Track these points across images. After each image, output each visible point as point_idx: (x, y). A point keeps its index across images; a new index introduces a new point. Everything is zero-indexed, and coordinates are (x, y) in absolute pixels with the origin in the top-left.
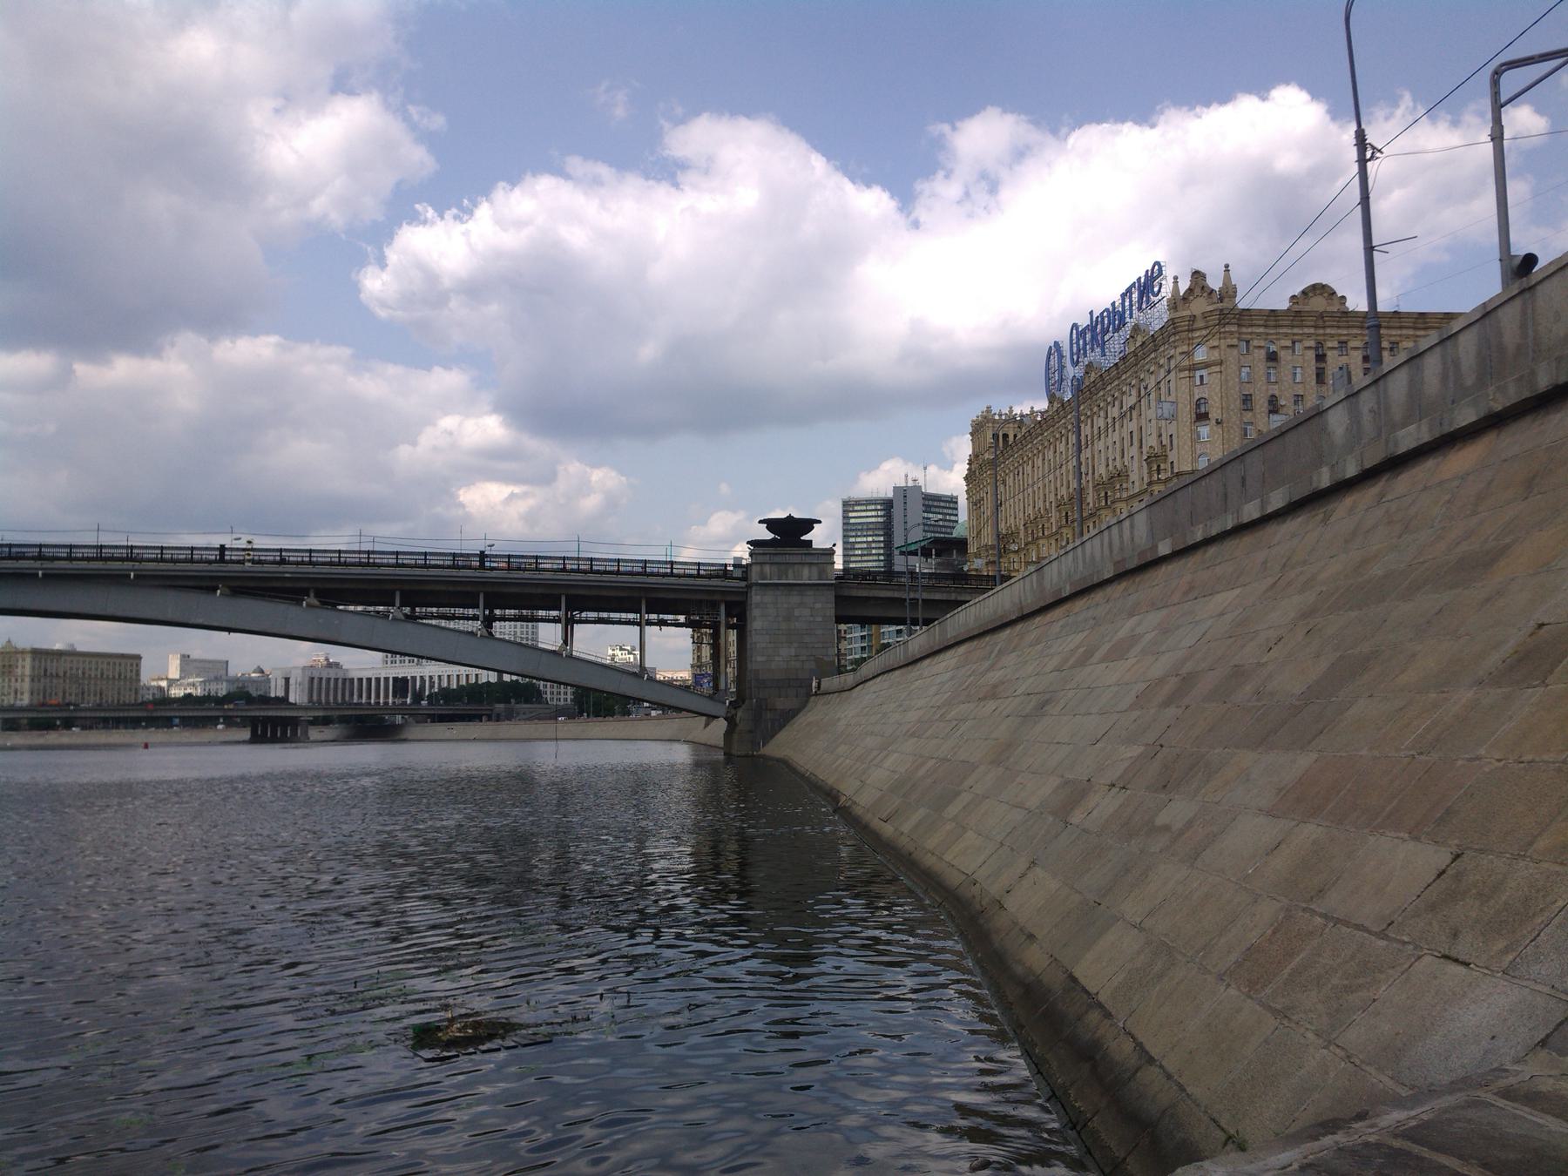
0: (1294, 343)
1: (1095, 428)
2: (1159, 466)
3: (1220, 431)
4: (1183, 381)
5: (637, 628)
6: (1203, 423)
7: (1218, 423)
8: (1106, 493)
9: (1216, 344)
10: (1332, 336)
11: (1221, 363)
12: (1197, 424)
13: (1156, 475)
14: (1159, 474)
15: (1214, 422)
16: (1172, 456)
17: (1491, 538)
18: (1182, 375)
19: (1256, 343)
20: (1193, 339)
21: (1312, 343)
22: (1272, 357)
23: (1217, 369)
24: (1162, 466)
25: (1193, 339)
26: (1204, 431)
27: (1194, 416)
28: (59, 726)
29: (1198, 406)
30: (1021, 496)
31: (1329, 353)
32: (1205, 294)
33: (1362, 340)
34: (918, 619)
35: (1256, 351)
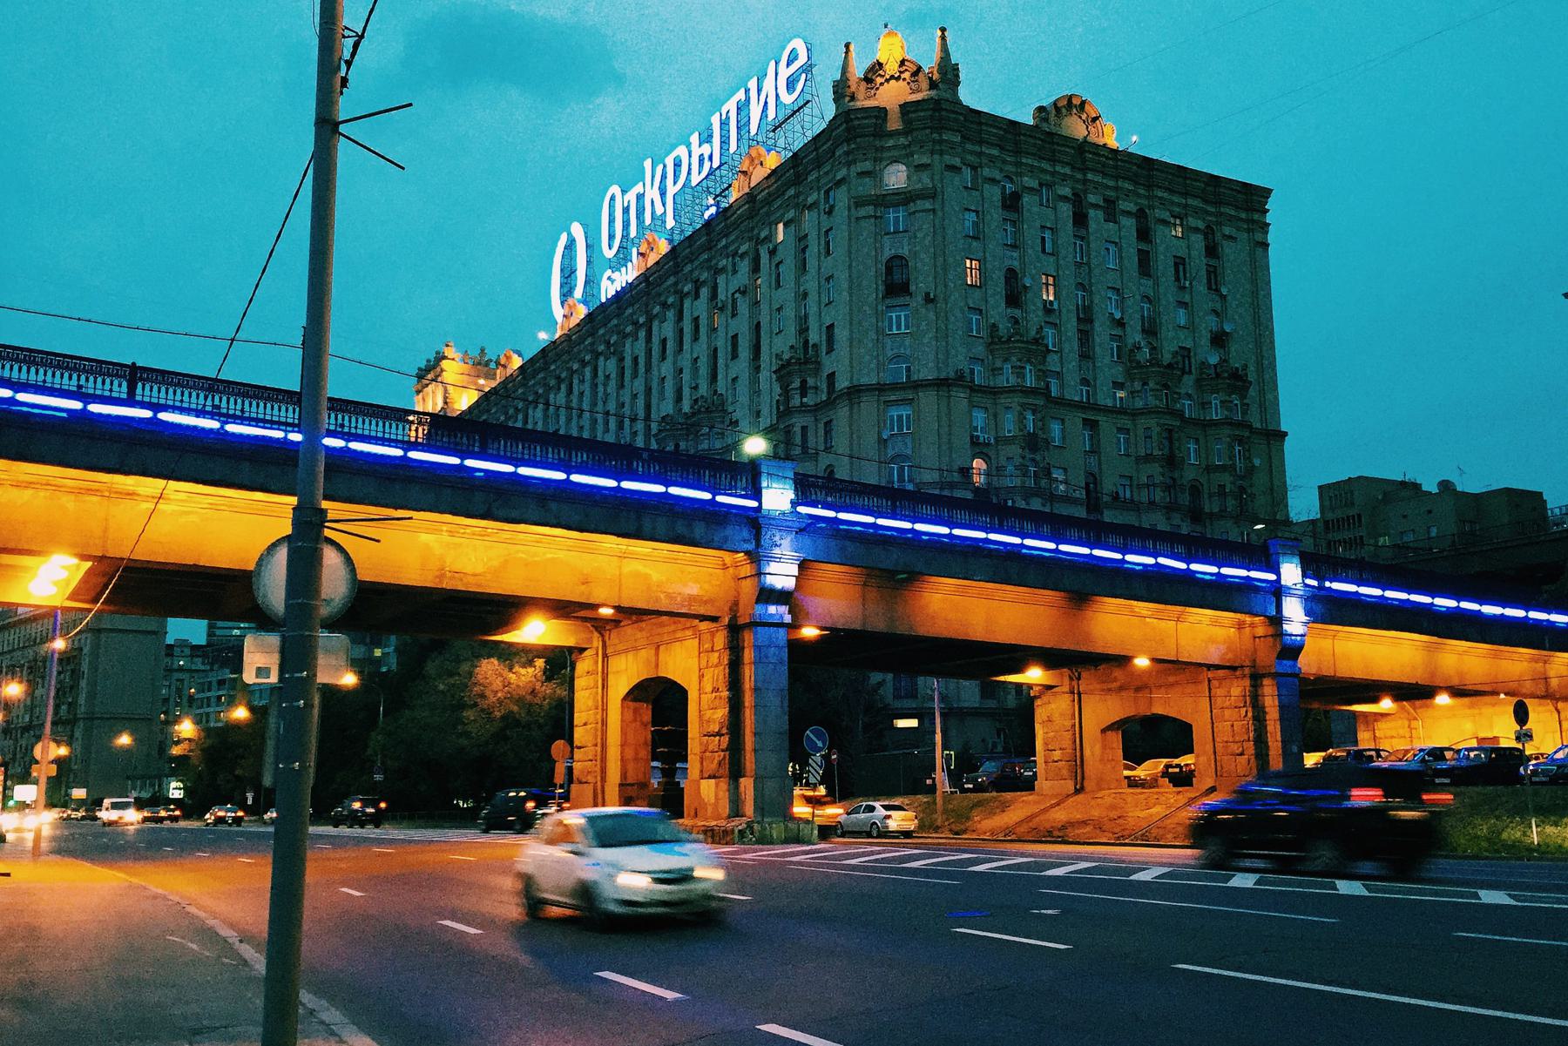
0: (1041, 185)
1: (656, 341)
2: (804, 382)
3: (932, 316)
4: (863, 223)
5: (339, 383)
6: (901, 301)
7: (928, 300)
8: (804, 382)
9: (925, 160)
10: (1097, 185)
11: (933, 196)
12: (888, 302)
13: (797, 397)
14: (803, 395)
15: (920, 299)
16: (828, 365)
17: (1115, 685)
18: (863, 212)
19: (986, 172)
20: (883, 149)
21: (1066, 191)
22: (1012, 203)
23: (928, 205)
24: (811, 382)
25: (883, 149)
26: (899, 320)
27: (882, 288)
28: (11, 808)
29: (889, 270)
30: (666, 369)
31: (1092, 213)
32: (907, 75)
33: (1136, 204)
35: (986, 186)
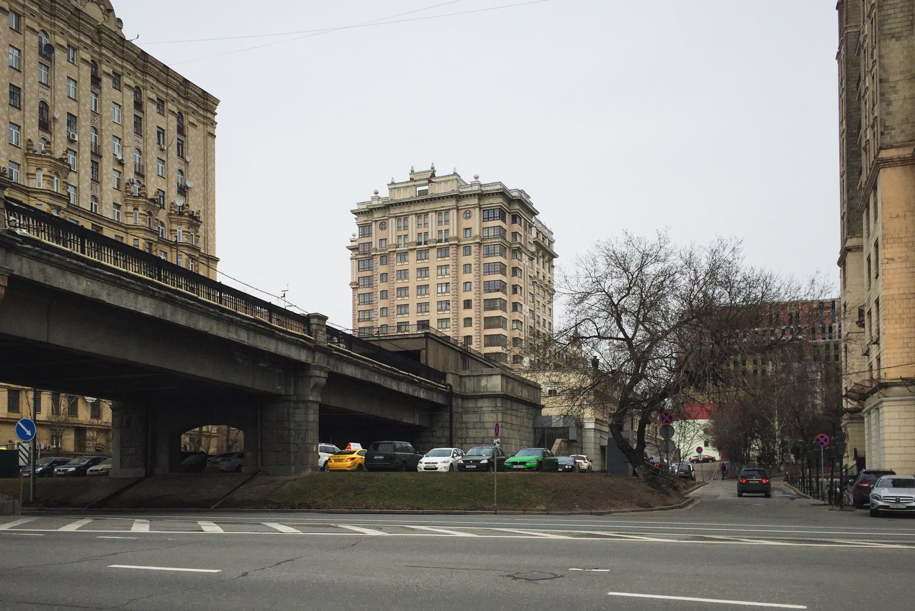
34: (442, 240)
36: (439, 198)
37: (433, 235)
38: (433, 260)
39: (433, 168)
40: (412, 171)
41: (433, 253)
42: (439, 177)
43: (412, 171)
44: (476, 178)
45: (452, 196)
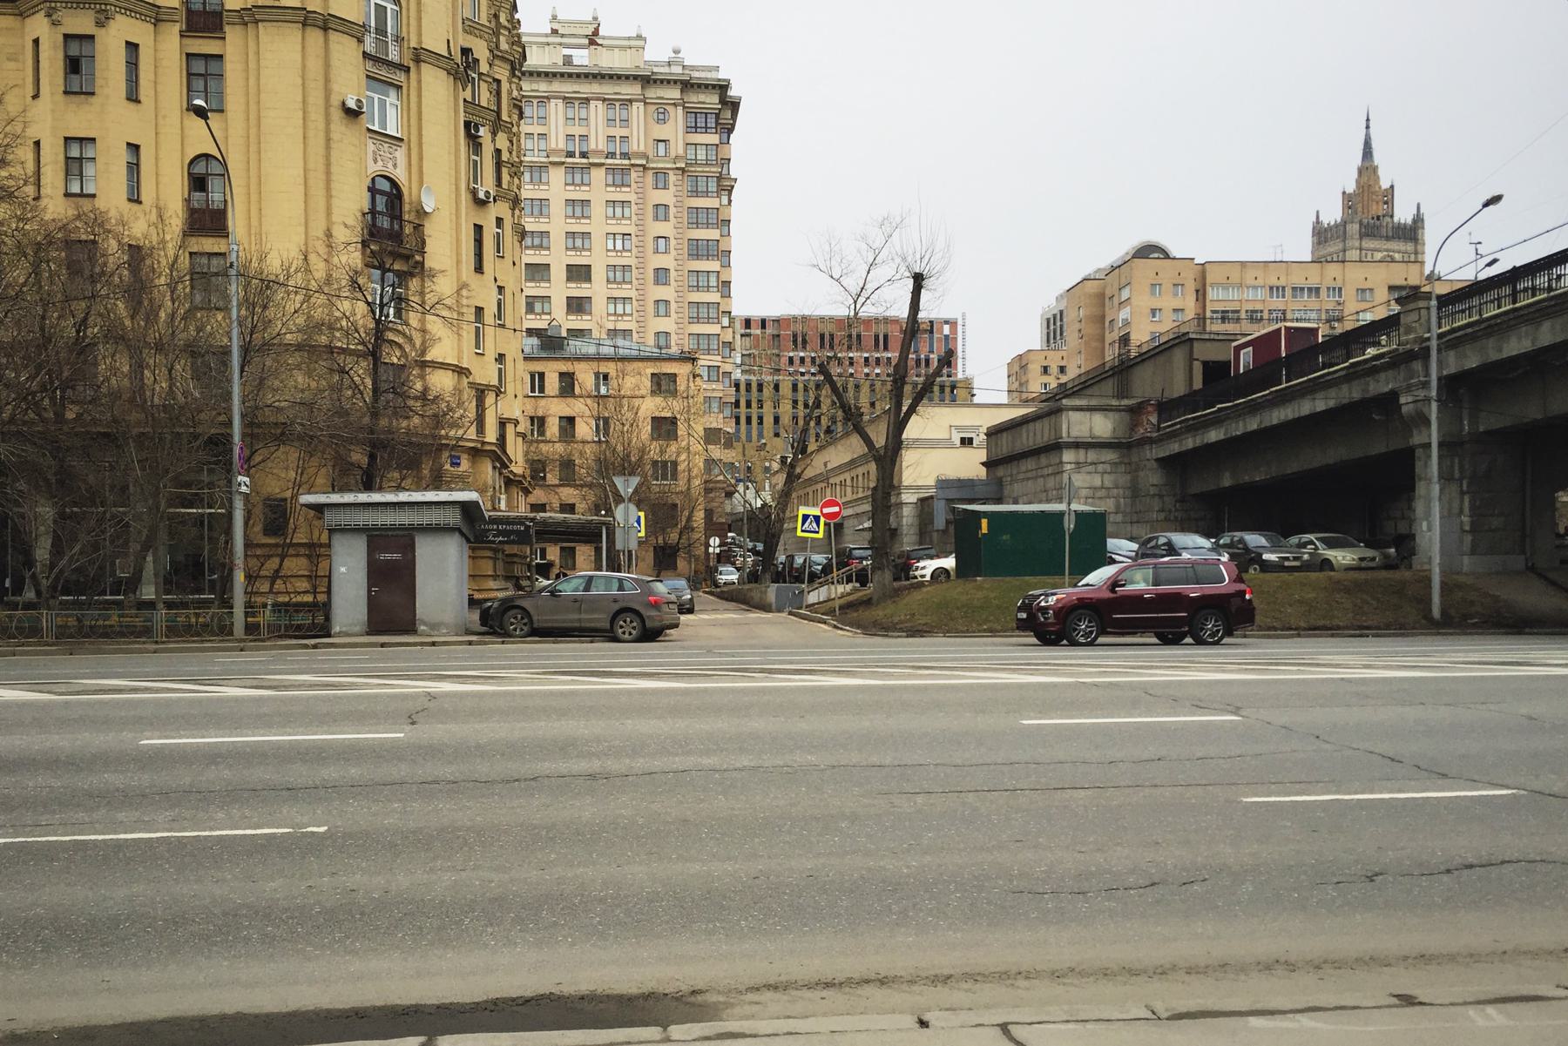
36: (611, 77)
37: (597, 142)
38: (598, 188)
39: (595, 19)
40: (554, 18)
41: (598, 175)
42: (604, 38)
43: (554, 18)
44: (677, 52)
45: (636, 77)
